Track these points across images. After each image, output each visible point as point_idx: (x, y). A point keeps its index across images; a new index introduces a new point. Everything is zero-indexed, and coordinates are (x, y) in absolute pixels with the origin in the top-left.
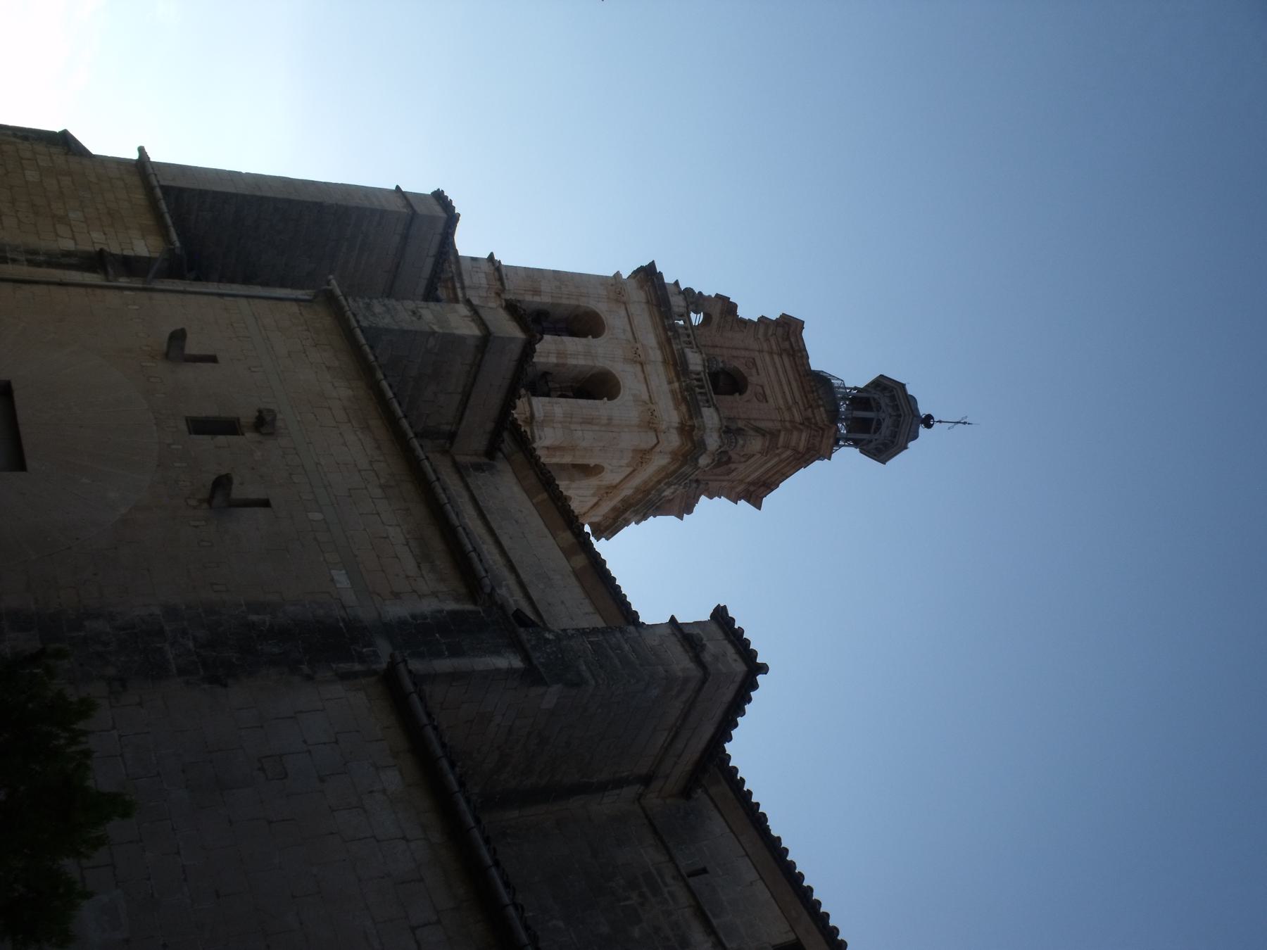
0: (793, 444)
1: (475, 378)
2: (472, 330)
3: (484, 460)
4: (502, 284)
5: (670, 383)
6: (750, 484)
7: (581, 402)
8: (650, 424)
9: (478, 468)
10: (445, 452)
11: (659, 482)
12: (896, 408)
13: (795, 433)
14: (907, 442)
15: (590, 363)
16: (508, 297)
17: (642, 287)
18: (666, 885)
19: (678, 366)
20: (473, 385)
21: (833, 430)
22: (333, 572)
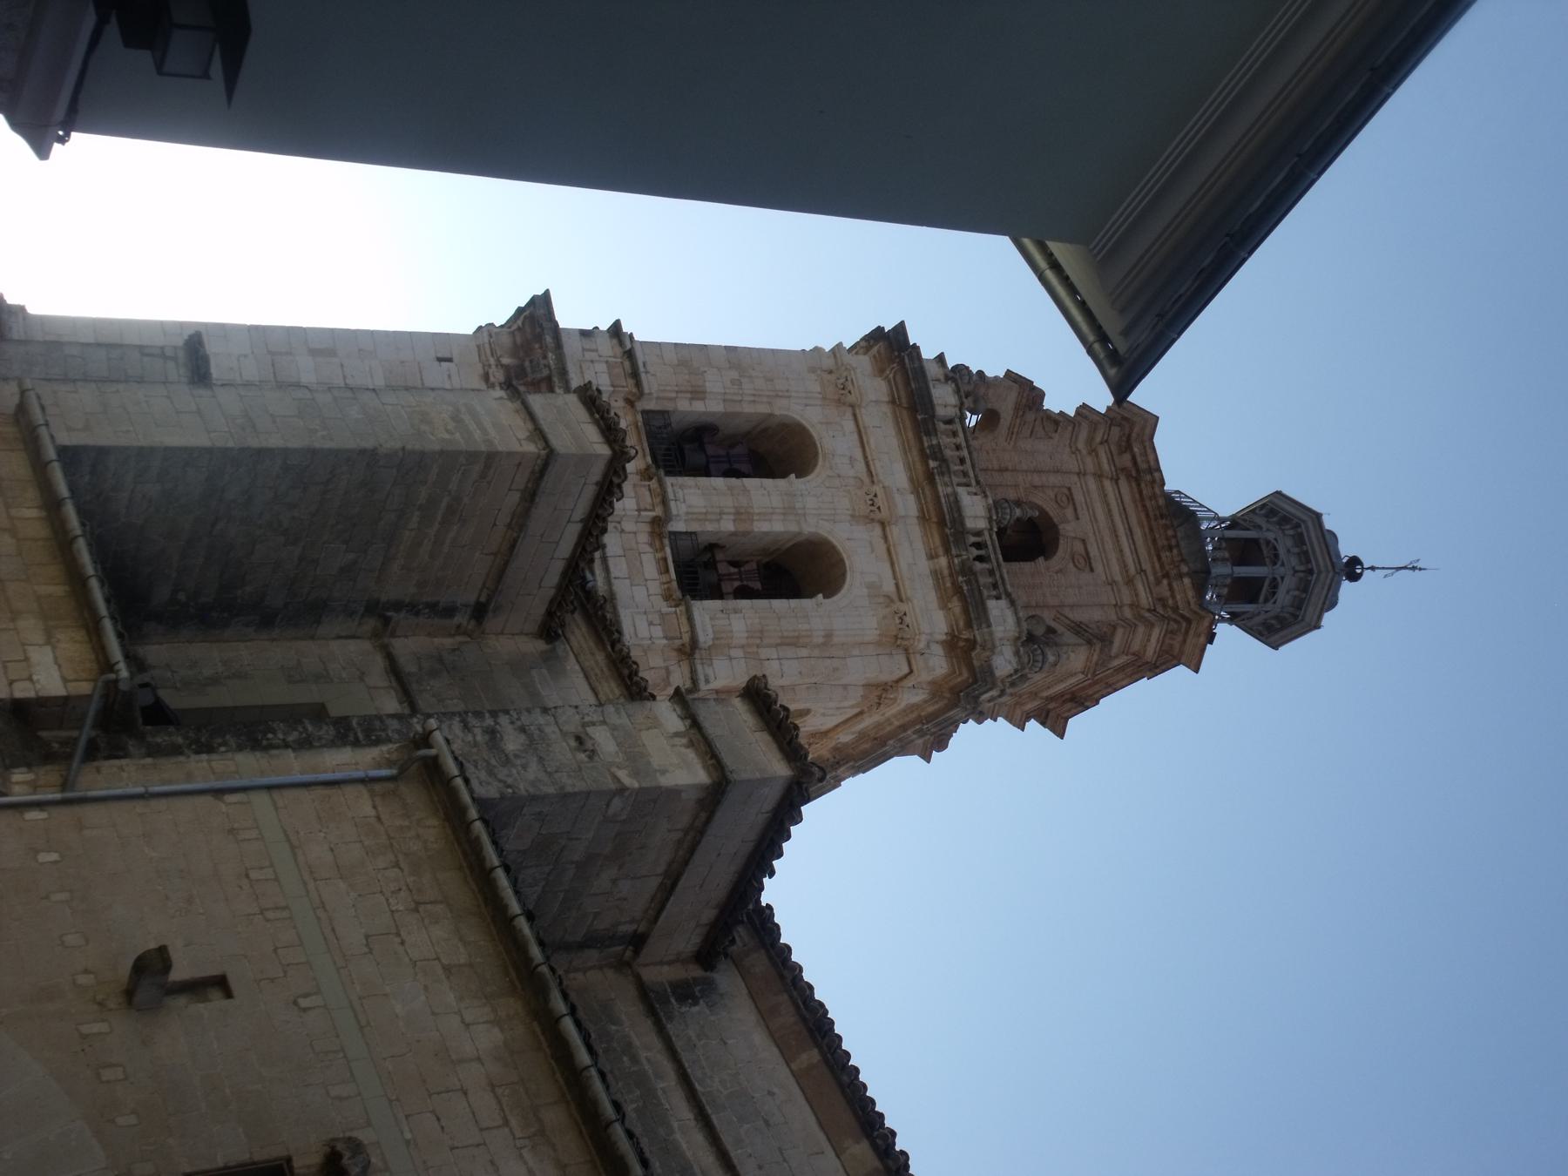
0: (1136, 647)
1: (692, 851)
2: (687, 773)
3: (696, 972)
4: (638, 384)
5: (932, 556)
6: (1051, 699)
7: (778, 604)
8: (898, 640)
9: (686, 993)
10: (622, 965)
11: (904, 728)
12: (1305, 557)
13: (1141, 629)
14: (1320, 618)
15: (793, 528)
17: (881, 372)
19: (945, 524)
20: (686, 863)
21: (1206, 623)
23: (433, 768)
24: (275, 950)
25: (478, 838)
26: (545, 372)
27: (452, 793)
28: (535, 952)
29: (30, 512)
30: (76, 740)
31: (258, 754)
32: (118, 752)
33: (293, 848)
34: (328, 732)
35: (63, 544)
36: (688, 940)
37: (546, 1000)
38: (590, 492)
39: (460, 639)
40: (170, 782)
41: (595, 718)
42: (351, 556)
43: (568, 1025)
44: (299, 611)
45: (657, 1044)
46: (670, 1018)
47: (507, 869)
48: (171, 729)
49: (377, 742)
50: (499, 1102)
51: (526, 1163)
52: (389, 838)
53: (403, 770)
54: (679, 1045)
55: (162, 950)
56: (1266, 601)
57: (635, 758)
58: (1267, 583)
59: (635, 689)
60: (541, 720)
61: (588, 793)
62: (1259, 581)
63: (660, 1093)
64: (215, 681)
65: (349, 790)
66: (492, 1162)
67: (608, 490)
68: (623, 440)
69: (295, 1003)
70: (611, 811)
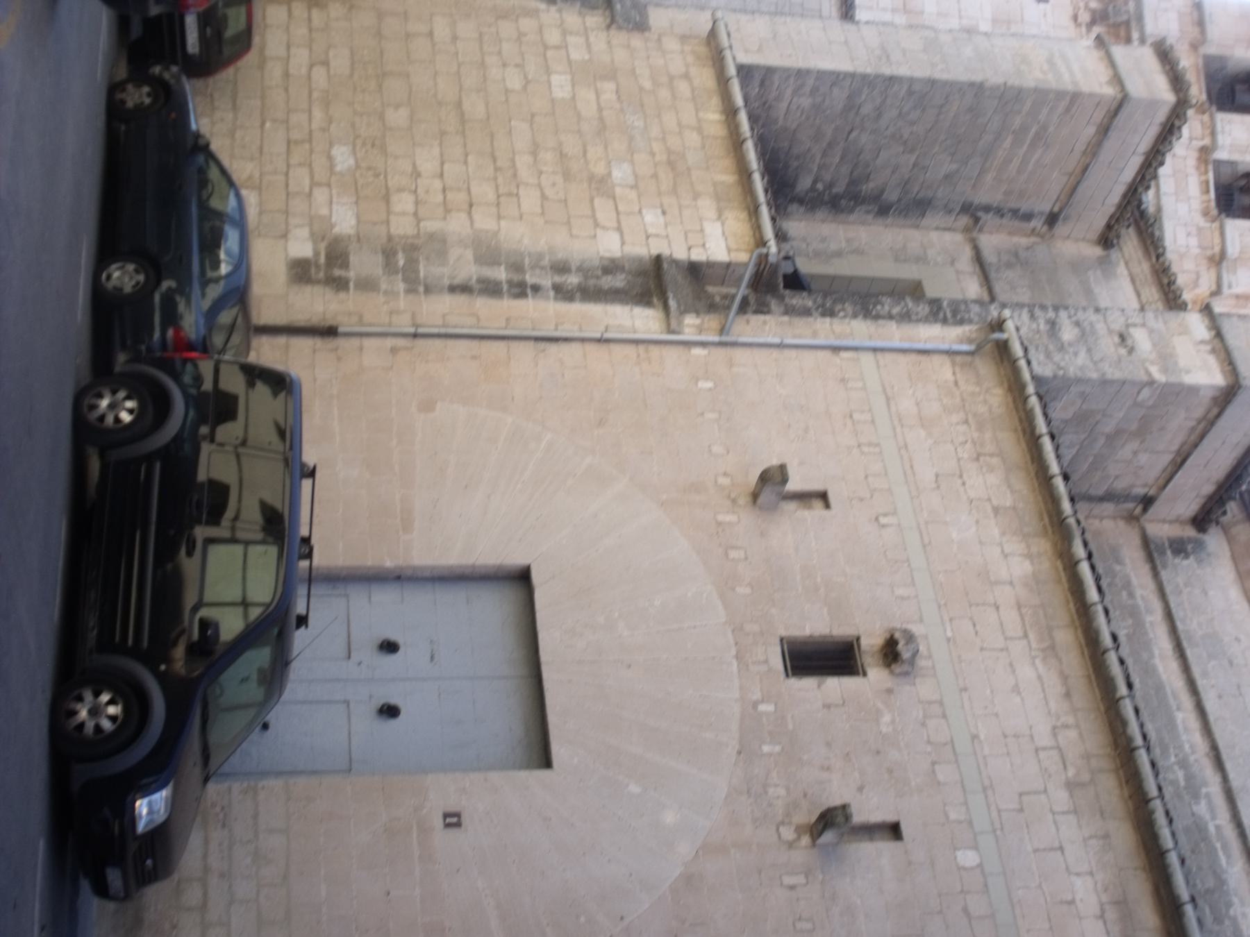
1: (1202, 437)
2: (1205, 374)
3: (1190, 532)
9: (1179, 548)
10: (1131, 518)
16: (1211, 50)
20: (1196, 445)
23: (1003, 348)
24: (866, 477)
25: (1032, 410)
26: (1125, 17)
27: (1016, 371)
28: (1066, 506)
29: (713, 116)
30: (733, 297)
31: (869, 322)
32: (762, 309)
33: (888, 399)
34: (923, 309)
35: (736, 144)
36: (1189, 506)
37: (1070, 545)
38: (1153, 132)
39: (1033, 239)
40: (800, 337)
41: (1138, 320)
42: (954, 167)
43: (1084, 567)
44: (913, 206)
45: (1151, 585)
46: (1165, 567)
47: (1053, 437)
48: (805, 294)
49: (961, 322)
50: (1023, 619)
51: (1036, 669)
52: (963, 400)
53: (979, 348)
54: (1168, 589)
55: (782, 468)
57: (1166, 358)
59: (1172, 299)
60: (1093, 317)
61: (1124, 382)
63: (1148, 625)
64: (839, 254)
65: (937, 359)
66: (1011, 665)
67: (1169, 131)
68: (1188, 89)
69: (877, 519)
70: (1141, 397)
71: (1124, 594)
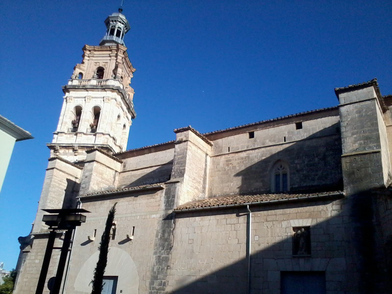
18: (230, 158)
22: (152, 217)
56: (121, 29)
58: (118, 29)
62: (118, 30)
71: (129, 177)
